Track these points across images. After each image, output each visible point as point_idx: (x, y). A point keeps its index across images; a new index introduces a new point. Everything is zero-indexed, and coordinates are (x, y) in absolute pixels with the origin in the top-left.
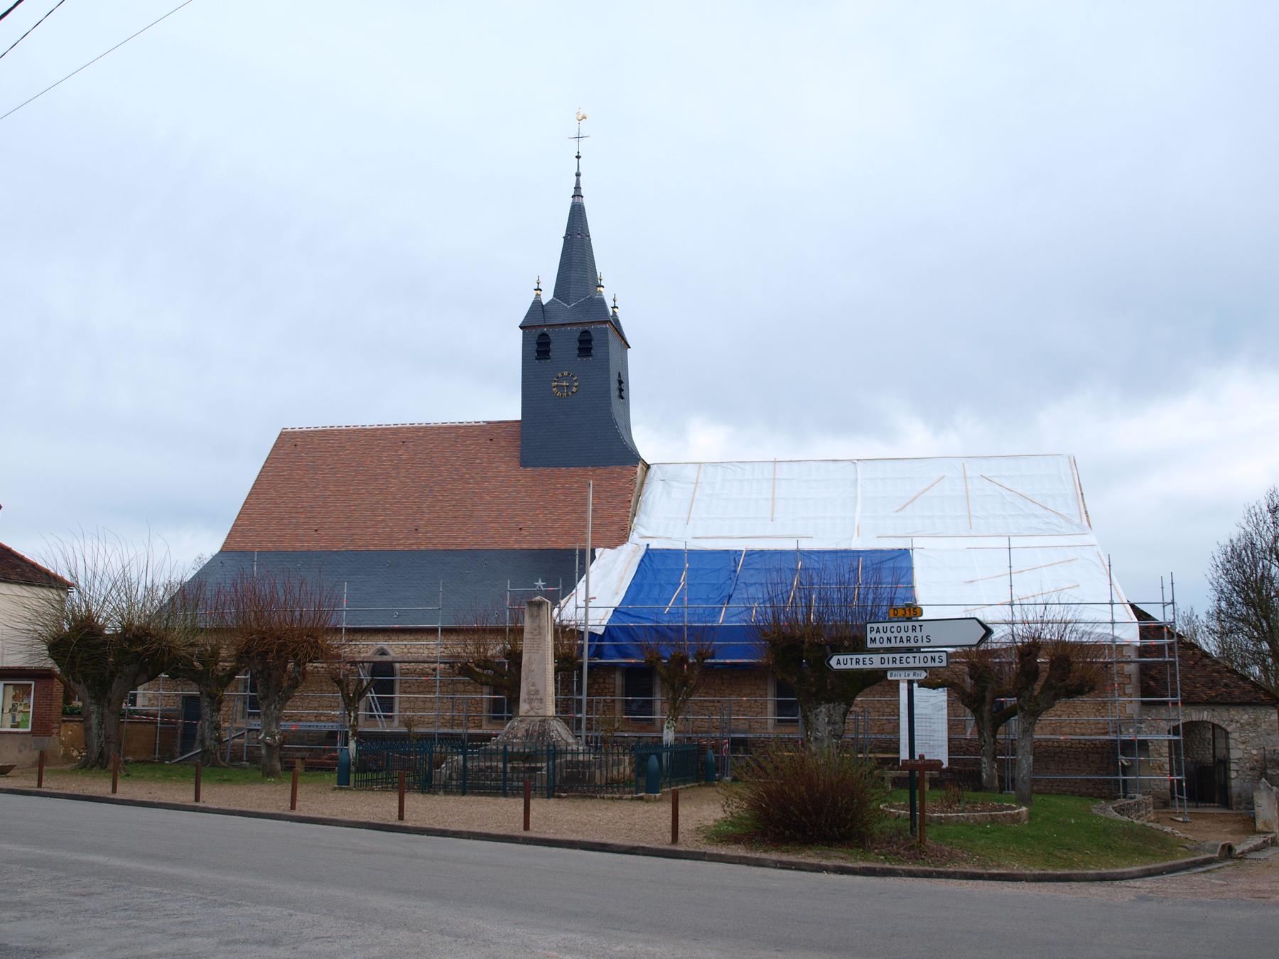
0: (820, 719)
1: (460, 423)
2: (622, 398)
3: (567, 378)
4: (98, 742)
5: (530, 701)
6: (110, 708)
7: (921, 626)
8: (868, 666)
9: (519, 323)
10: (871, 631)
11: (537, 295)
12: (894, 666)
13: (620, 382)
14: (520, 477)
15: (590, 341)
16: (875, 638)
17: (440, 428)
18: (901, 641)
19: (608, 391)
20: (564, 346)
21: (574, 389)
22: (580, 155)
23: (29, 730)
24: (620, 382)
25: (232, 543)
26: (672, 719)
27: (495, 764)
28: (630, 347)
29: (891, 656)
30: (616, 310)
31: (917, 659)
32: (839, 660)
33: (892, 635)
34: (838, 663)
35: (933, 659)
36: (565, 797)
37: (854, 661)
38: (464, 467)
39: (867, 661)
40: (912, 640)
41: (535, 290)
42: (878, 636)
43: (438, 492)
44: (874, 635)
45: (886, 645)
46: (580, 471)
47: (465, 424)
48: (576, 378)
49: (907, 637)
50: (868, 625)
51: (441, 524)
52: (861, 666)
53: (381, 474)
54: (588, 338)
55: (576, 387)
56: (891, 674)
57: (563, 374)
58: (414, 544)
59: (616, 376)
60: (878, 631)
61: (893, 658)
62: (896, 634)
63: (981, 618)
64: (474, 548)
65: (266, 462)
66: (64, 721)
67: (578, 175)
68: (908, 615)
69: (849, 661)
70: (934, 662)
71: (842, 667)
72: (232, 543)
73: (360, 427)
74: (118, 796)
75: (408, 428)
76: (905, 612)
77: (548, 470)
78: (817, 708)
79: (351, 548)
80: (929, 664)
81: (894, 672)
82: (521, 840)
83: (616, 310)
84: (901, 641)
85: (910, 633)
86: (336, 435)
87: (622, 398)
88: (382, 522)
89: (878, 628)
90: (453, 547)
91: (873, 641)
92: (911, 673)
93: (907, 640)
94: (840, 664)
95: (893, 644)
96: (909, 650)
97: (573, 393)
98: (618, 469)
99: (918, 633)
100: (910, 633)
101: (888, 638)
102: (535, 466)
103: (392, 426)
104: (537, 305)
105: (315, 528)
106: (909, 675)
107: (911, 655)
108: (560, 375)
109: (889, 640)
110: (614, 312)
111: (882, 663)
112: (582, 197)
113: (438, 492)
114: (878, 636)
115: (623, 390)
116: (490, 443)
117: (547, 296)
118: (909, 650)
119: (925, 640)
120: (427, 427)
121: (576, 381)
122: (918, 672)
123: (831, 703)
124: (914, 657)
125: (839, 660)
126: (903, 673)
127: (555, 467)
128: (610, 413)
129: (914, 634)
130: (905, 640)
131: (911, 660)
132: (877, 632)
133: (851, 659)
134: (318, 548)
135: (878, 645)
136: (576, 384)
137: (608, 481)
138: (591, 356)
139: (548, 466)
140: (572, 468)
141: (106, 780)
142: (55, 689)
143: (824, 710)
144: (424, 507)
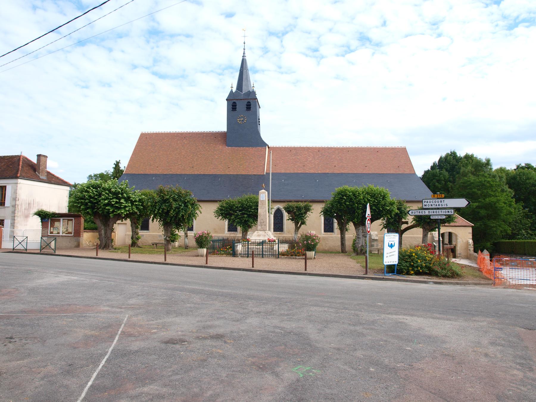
3: (243, 117)
4: (105, 240)
6: (109, 227)
8: (423, 214)
9: (226, 98)
10: (425, 202)
11: (232, 89)
12: (434, 214)
16: (426, 205)
17: (197, 133)
18: (436, 205)
20: (241, 106)
21: (245, 121)
23: (72, 235)
25: (128, 171)
29: (432, 211)
31: (442, 212)
32: (412, 212)
33: (433, 204)
35: (448, 212)
37: (418, 212)
39: (423, 212)
40: (440, 205)
42: (427, 204)
43: (199, 155)
44: (426, 203)
46: (247, 148)
47: (206, 132)
48: (245, 117)
50: (423, 200)
51: (201, 165)
52: (421, 214)
53: (178, 148)
56: (432, 217)
60: (427, 202)
62: (434, 203)
64: (214, 174)
65: (137, 143)
66: (84, 232)
67: (244, 49)
72: (128, 171)
73: (169, 132)
74: (130, 259)
75: (186, 133)
77: (236, 148)
79: (171, 173)
80: (447, 213)
81: (433, 216)
82: (308, 274)
84: (436, 205)
85: (440, 203)
86: (161, 135)
88: (180, 164)
90: (207, 173)
92: (440, 216)
95: (433, 207)
96: (438, 209)
97: (244, 122)
98: (260, 148)
99: (443, 203)
100: (440, 203)
102: (231, 147)
103: (180, 132)
104: (232, 91)
105: (157, 166)
106: (439, 217)
107: (440, 210)
108: (240, 116)
109: (432, 205)
113: (199, 155)
114: (427, 204)
117: (234, 90)
118: (438, 209)
120: (204, 133)
121: (245, 118)
122: (442, 216)
125: (412, 212)
126: (436, 216)
129: (441, 203)
130: (438, 205)
131: (440, 212)
133: (417, 212)
134: (159, 173)
136: (246, 119)
138: (236, 111)
139: (236, 147)
140: (245, 148)
141: (95, 252)
142: (81, 221)
143: (361, 228)
144: (195, 160)
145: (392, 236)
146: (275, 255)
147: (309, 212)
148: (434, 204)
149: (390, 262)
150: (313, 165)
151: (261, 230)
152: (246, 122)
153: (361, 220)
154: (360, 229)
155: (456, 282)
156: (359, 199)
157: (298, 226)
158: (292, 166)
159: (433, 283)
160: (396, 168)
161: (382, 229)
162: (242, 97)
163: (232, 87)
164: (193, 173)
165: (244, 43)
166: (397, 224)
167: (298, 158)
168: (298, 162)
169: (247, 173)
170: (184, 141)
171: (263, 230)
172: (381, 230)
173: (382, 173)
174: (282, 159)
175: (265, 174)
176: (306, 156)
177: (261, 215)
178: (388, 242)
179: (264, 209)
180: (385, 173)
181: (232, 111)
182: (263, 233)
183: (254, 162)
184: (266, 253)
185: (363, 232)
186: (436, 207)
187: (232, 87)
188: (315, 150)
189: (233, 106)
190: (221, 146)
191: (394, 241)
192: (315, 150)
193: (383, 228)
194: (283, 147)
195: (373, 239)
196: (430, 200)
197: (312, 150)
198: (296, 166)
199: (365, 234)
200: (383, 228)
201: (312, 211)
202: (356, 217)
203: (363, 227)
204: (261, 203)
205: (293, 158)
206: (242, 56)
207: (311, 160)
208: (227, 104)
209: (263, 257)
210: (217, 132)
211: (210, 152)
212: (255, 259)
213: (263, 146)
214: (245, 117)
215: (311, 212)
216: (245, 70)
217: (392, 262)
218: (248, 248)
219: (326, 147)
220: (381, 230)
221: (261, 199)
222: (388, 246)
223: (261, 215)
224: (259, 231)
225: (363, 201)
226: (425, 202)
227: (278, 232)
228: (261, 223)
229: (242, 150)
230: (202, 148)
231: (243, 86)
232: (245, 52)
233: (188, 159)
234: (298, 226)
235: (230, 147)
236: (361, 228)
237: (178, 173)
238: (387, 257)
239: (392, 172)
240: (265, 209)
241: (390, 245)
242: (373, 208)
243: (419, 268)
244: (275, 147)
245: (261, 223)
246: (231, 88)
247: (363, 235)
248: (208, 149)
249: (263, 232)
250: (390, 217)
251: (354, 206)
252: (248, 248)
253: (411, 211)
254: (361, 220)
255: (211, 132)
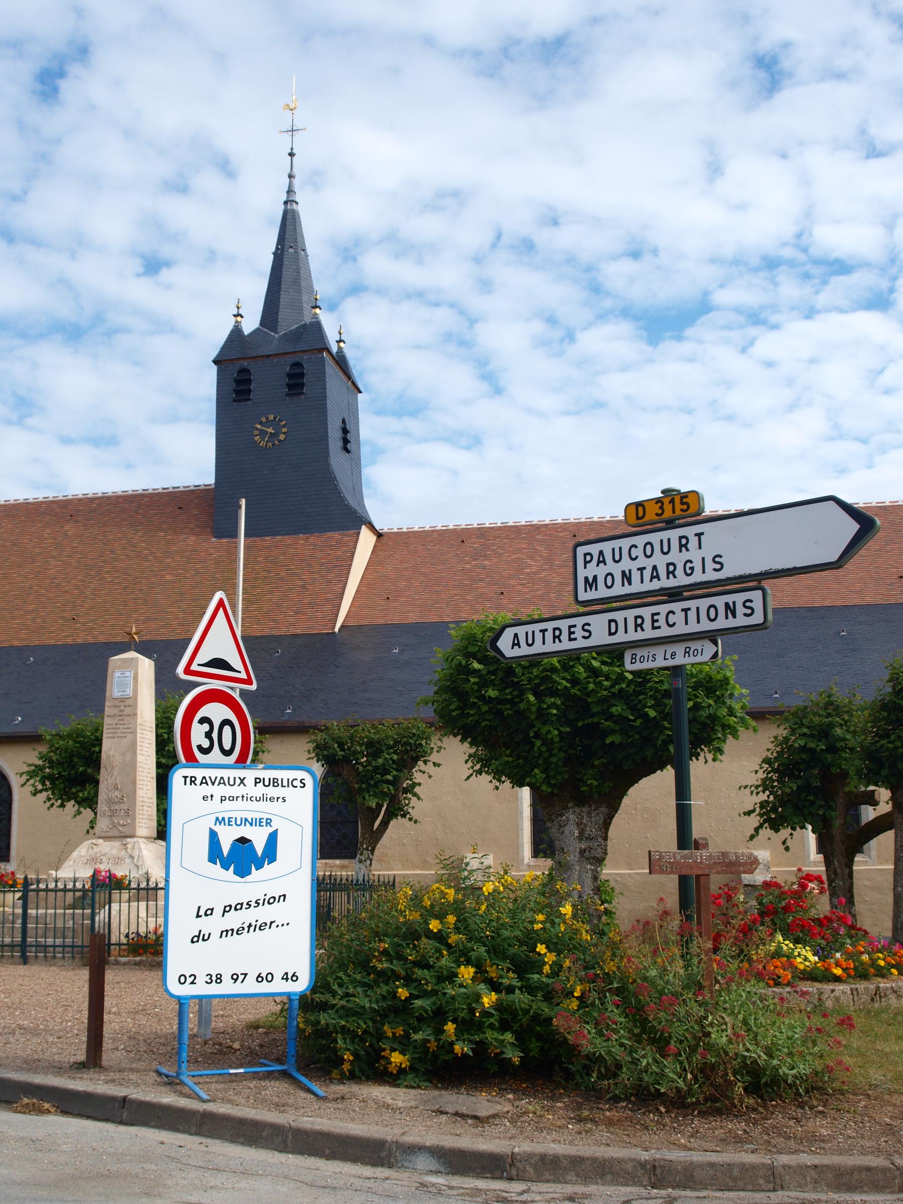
0: (567, 832)
1: (144, 490)
2: (348, 451)
3: (275, 423)
5: (113, 814)
7: (699, 535)
9: (212, 358)
10: (586, 563)
11: (237, 322)
12: (640, 635)
13: (345, 431)
14: (211, 551)
15: (249, 381)
16: (595, 577)
17: (119, 497)
18: (655, 576)
19: (324, 437)
21: (282, 437)
22: (294, 151)
24: (345, 431)
26: (367, 849)
27: (40, 911)
28: (360, 392)
29: (631, 614)
30: (342, 344)
31: (692, 615)
32: (516, 636)
33: (634, 566)
34: (516, 644)
36: (125, 964)
37: (549, 635)
38: (143, 541)
40: (679, 572)
41: (235, 316)
43: (108, 572)
44: (592, 570)
45: (619, 590)
46: (289, 540)
48: (284, 422)
49: (668, 565)
54: (299, 371)
55: (284, 433)
56: (633, 657)
57: (267, 419)
58: (69, 636)
59: (339, 424)
60: (602, 561)
61: (636, 617)
62: (642, 561)
63: (848, 499)
67: (291, 176)
68: (668, 513)
69: (538, 636)
70: (734, 616)
71: (524, 650)
76: (661, 508)
78: (562, 815)
81: (640, 652)
83: (342, 344)
84: (655, 576)
85: (676, 556)
87: (348, 451)
89: (601, 553)
91: (591, 583)
92: (679, 649)
93: (668, 573)
94: (518, 645)
95: (636, 587)
96: (674, 595)
97: (280, 441)
98: (336, 535)
99: (694, 554)
100: (676, 556)
101: (623, 572)
104: (237, 331)
106: (673, 655)
107: (677, 606)
108: (264, 419)
109: (627, 577)
110: (340, 348)
111: (610, 634)
112: (297, 203)
113: (108, 572)
114: (601, 571)
115: (349, 442)
116: (180, 511)
117: (251, 324)
119: (710, 565)
121: (284, 426)
122: (694, 645)
123: (583, 806)
124: (686, 610)
125: (516, 636)
126: (659, 651)
127: (258, 536)
128: (328, 465)
129: (685, 556)
130: (662, 572)
131: (679, 618)
132: (599, 562)
133: (543, 631)
135: (602, 592)
136: (285, 430)
137: (323, 550)
138: (249, 399)
140: (279, 537)
143: (571, 817)
145: (250, 782)
146: (51, 949)
147: (425, 762)
148: (641, 569)
149: (227, 978)
150: (538, 590)
151: (110, 834)
152: (285, 439)
153: (566, 776)
154: (568, 819)
155: (642, 1165)
156: (544, 670)
157: (375, 827)
158: (456, 595)
159: (433, 1164)
160: (890, 584)
161: (757, 830)
162: (272, 349)
163: (238, 315)
164: (69, 641)
165: (291, 155)
166: (823, 803)
167: (484, 567)
168: (481, 580)
169: (267, 632)
170: (66, 528)
171: (117, 834)
172: (752, 837)
173: (827, 603)
174: (423, 574)
175: (337, 630)
176: (518, 559)
177: (113, 767)
178: (210, 823)
179: (125, 740)
180: (839, 603)
181: (234, 401)
182: (112, 848)
183: (304, 587)
184: (50, 941)
185: (581, 838)
186: (656, 585)
187: (238, 315)
188: (561, 534)
189: (238, 382)
190: (193, 538)
191: (269, 822)
192: (561, 534)
193: (761, 826)
194: (438, 528)
195: (747, 883)
196: (616, 544)
197: (548, 533)
198: (469, 597)
199: (590, 844)
200: (761, 826)
201: (434, 757)
202: (540, 762)
203: (584, 809)
204: (116, 711)
205: (467, 566)
206: (285, 199)
207: (535, 569)
208: (218, 379)
209: (25, 960)
210: (192, 488)
211: (149, 561)
212: (110, 976)
213: (347, 528)
214: (284, 422)
215: (435, 764)
216: (290, 250)
217: (251, 978)
218: (25, 915)
219: (608, 522)
220: (752, 837)
221: (117, 693)
222: (212, 859)
223: (113, 767)
224: (101, 841)
225: (564, 679)
226: (586, 563)
227: (338, 862)
228: (110, 802)
229: (268, 548)
230: (125, 548)
231: (281, 310)
232: (296, 188)
233: (66, 592)
234: (375, 827)
235: (224, 540)
236: (571, 817)
237: (16, 643)
238: (199, 938)
239: (869, 598)
240: (130, 736)
241: (226, 848)
242: (613, 709)
243: (450, 1027)
244: (404, 530)
245: (110, 802)
246: (234, 319)
247: (582, 852)
248: (146, 549)
249: (116, 844)
250: (607, 742)
251: (522, 706)
252: (25, 915)
253: (507, 630)
254: (566, 776)
255: (171, 490)
